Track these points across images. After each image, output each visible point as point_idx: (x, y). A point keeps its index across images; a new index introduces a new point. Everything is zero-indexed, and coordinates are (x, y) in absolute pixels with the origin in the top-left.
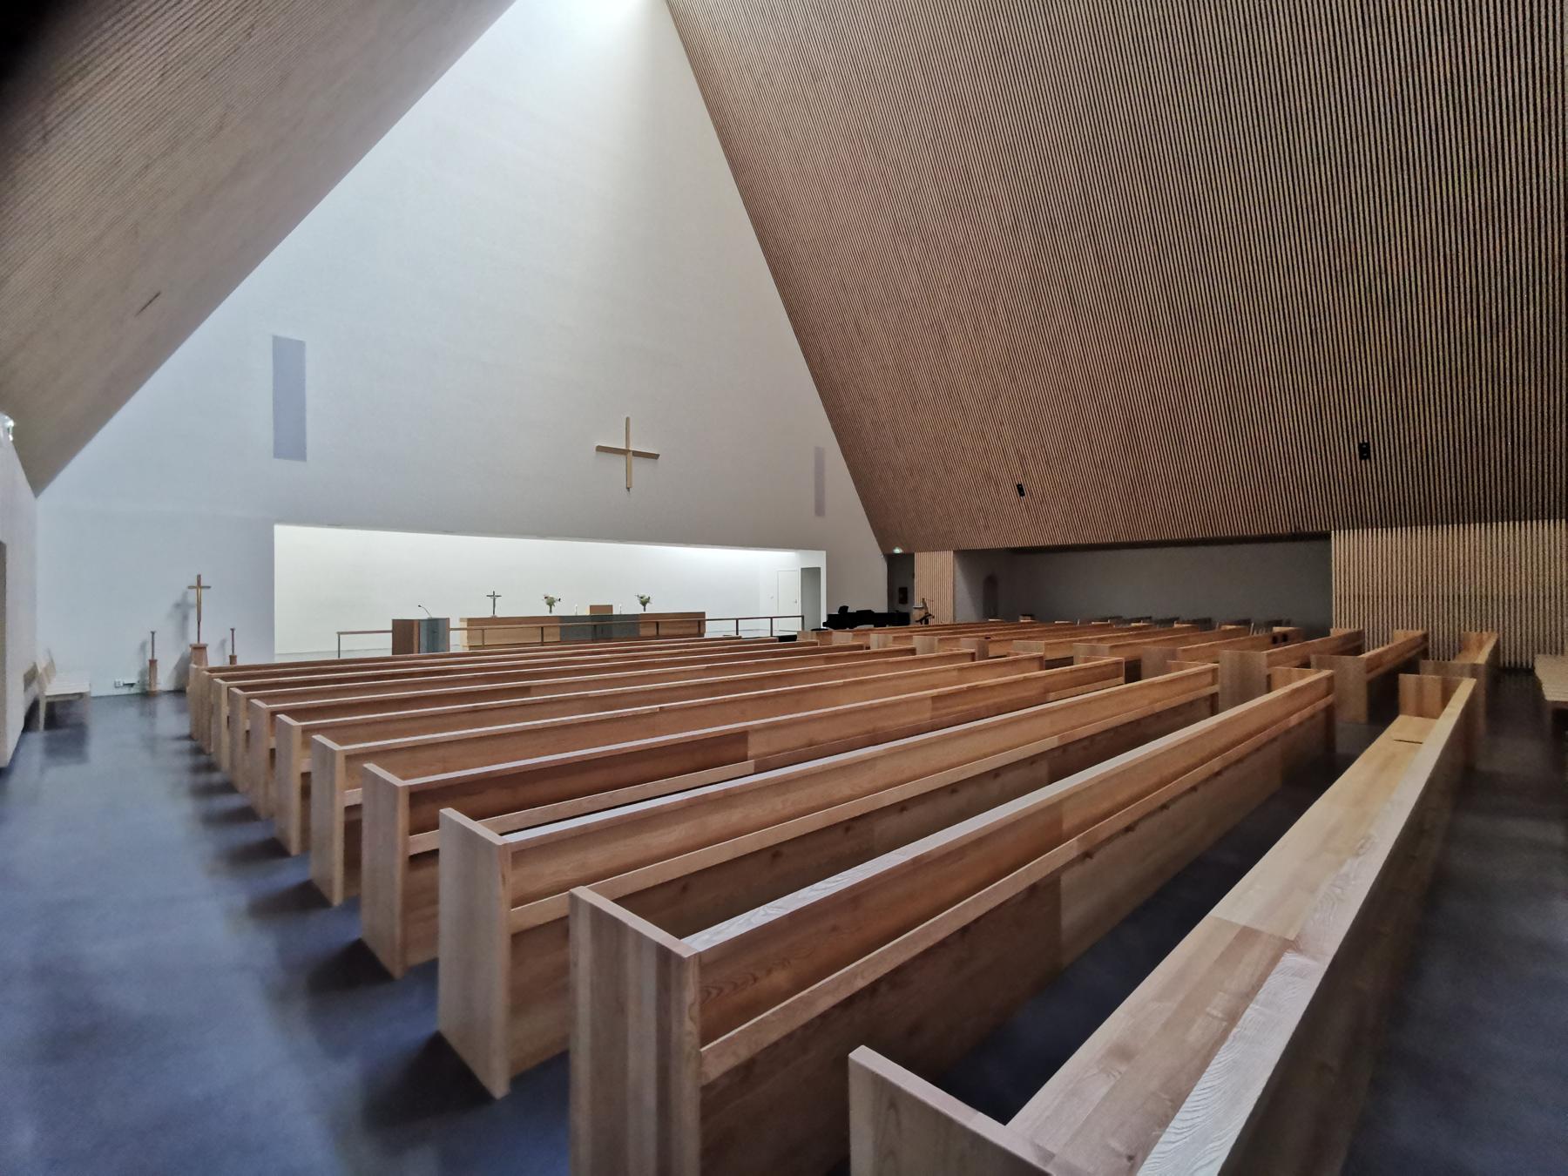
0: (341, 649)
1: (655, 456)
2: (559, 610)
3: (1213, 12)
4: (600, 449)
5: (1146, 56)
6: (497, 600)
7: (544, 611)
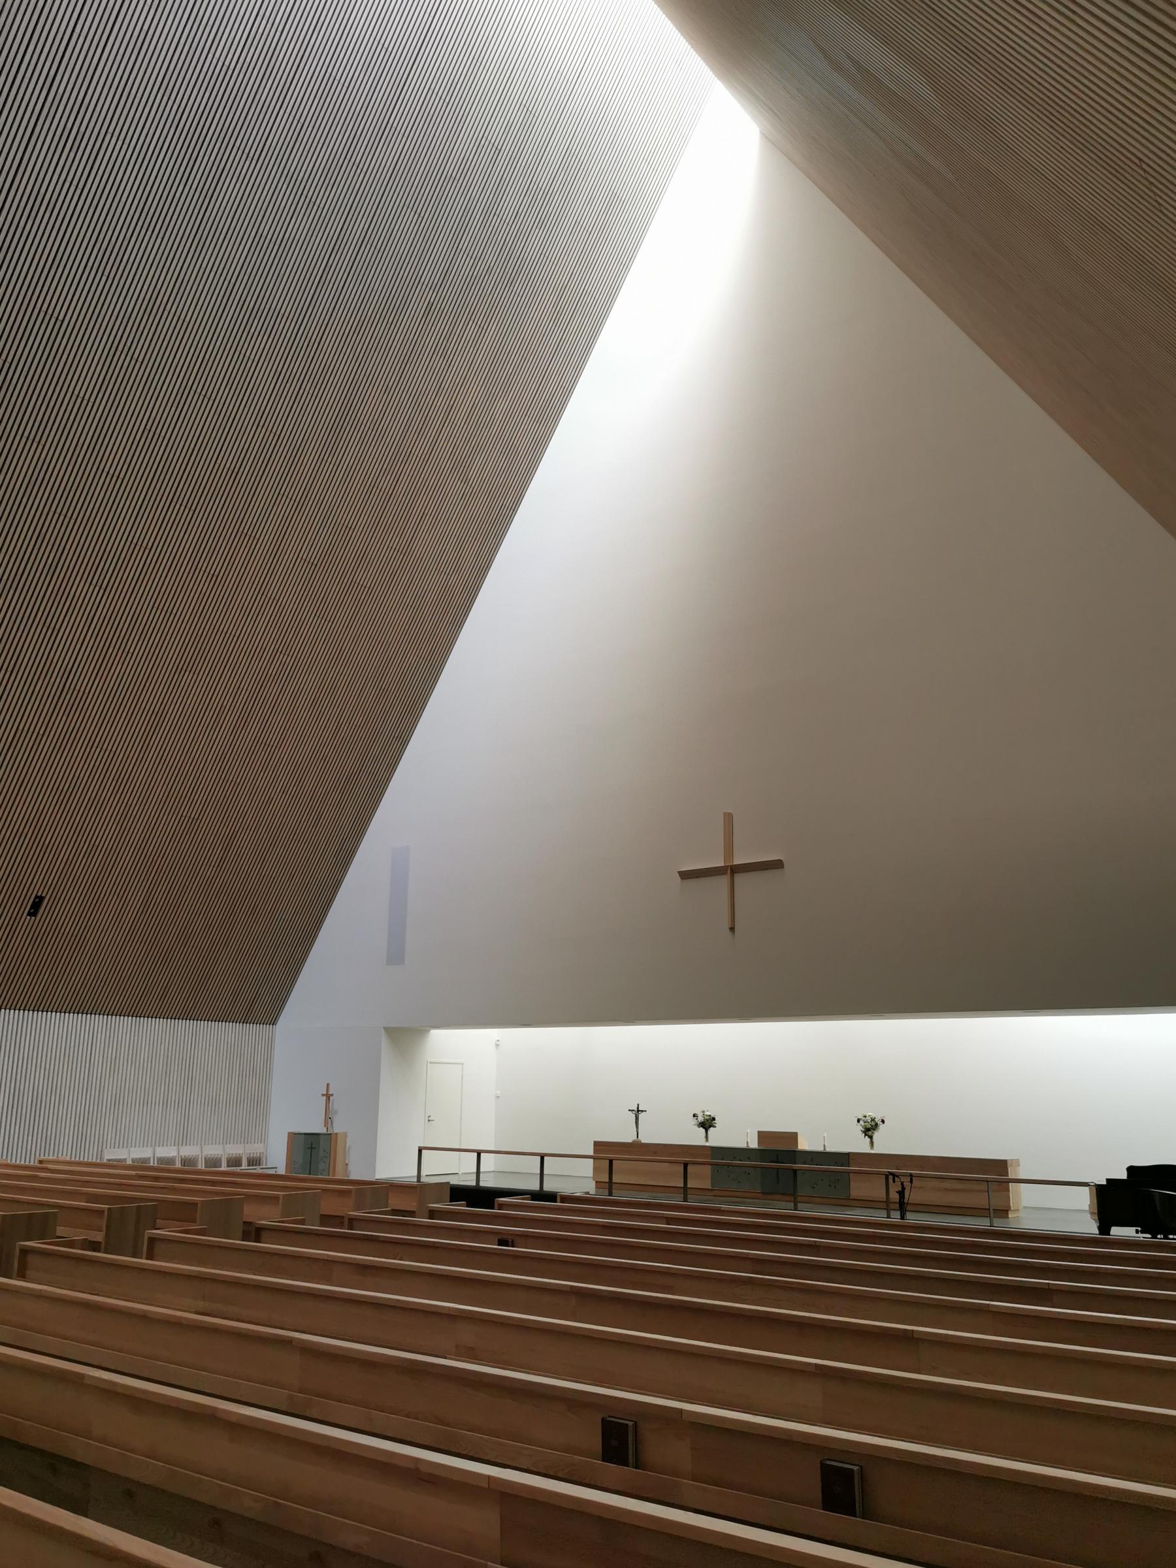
0: (482, 1170)
1: (777, 865)
2: (719, 1138)
3: (335, 742)
4: (685, 875)
5: (898, 65)
6: (641, 1116)
7: (695, 1137)
